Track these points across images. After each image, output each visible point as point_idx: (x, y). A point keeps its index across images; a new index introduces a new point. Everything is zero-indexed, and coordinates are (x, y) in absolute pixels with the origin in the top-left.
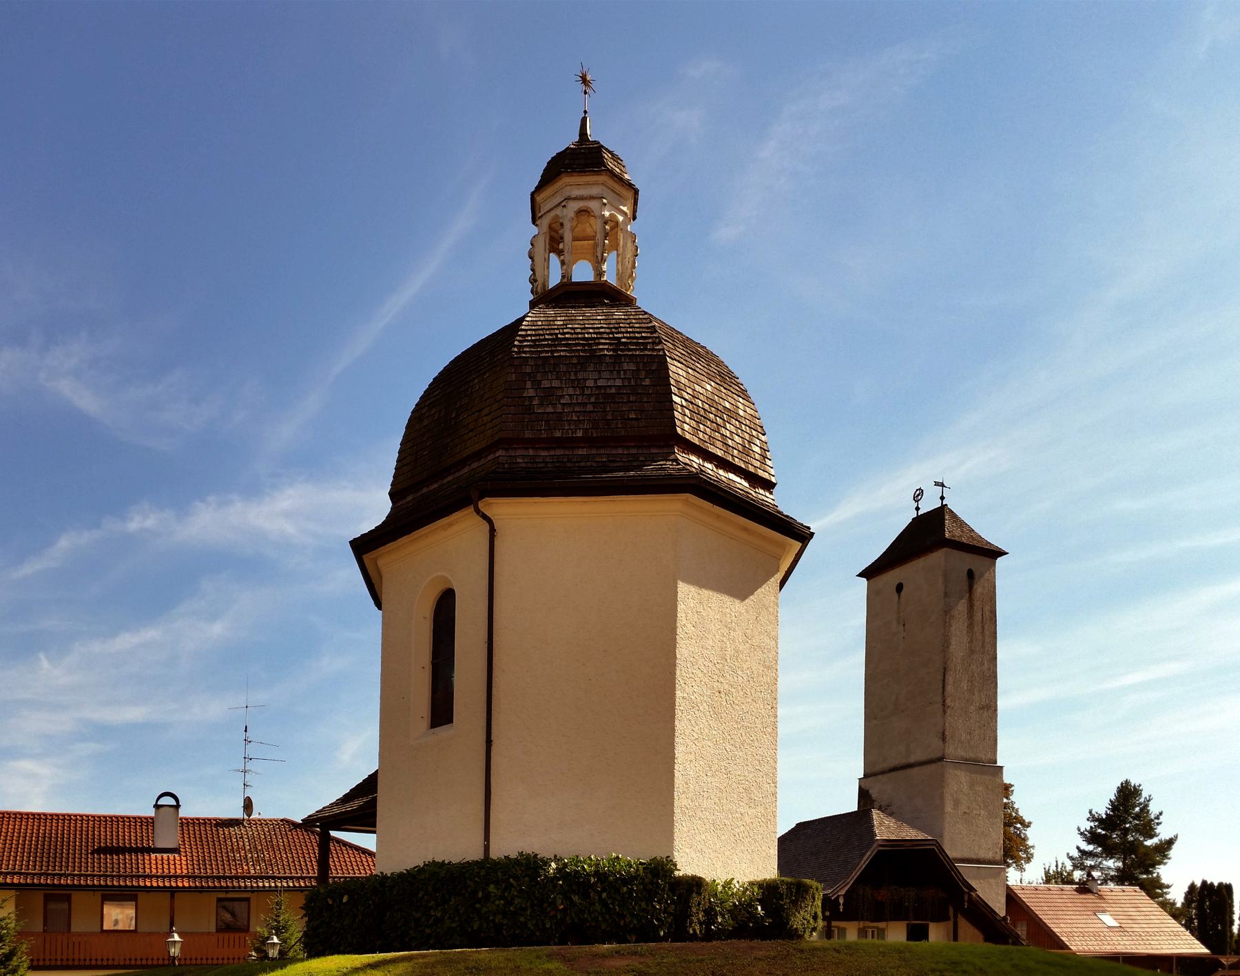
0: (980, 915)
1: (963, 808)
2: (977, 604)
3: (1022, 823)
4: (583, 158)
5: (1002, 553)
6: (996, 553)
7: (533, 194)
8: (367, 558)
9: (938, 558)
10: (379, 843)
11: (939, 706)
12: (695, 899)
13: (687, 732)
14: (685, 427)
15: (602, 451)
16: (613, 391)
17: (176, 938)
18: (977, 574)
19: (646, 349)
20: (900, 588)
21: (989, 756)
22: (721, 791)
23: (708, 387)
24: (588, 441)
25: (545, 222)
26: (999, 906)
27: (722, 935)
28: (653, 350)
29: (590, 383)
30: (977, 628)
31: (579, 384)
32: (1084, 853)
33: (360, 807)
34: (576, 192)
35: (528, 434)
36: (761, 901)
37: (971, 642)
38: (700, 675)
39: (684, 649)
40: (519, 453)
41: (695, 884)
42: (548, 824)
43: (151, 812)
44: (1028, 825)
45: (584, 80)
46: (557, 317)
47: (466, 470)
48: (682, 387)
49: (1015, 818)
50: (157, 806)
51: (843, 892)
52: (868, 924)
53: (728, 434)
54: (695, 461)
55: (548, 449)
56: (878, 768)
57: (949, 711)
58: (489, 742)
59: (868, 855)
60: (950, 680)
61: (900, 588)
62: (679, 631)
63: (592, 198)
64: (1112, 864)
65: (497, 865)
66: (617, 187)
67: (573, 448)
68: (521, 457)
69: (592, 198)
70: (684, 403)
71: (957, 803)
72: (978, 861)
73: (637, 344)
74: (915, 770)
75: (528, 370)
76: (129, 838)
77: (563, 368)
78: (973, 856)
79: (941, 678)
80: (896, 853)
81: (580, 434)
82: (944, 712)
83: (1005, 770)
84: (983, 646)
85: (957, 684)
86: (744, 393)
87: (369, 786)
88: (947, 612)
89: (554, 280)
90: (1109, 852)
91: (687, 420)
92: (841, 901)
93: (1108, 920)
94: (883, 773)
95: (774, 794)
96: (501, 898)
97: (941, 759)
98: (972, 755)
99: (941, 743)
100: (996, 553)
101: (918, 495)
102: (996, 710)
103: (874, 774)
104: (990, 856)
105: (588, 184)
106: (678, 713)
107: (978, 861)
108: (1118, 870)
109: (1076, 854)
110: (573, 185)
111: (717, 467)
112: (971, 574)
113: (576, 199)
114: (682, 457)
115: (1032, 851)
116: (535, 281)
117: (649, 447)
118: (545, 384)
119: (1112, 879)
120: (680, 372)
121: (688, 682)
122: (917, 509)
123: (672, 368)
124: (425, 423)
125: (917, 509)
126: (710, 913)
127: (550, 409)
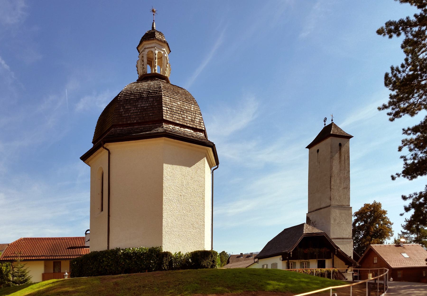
1: (337, 221)
2: (343, 154)
3: (390, 223)
4: (150, 36)
5: (351, 137)
6: (349, 137)
7: (137, 48)
9: (329, 140)
11: (329, 189)
12: (165, 259)
13: (168, 209)
14: (167, 116)
15: (142, 126)
16: (146, 107)
17: (67, 274)
18: (342, 144)
19: (157, 94)
20: (318, 151)
21: (347, 204)
22: (182, 225)
24: (138, 123)
27: (176, 268)
28: (159, 94)
29: (139, 106)
30: (343, 162)
31: (136, 106)
32: (404, 233)
34: (148, 46)
35: (120, 123)
36: (191, 258)
37: (340, 167)
38: (173, 191)
39: (166, 184)
40: (118, 128)
41: (167, 254)
42: (127, 239)
43: (84, 236)
44: (391, 224)
45: (153, 11)
46: (145, 85)
48: (167, 104)
49: (388, 222)
50: (86, 234)
51: (292, 251)
52: (303, 260)
53: (185, 117)
54: (171, 126)
55: (126, 127)
56: (312, 210)
57: (332, 190)
59: (300, 239)
60: (333, 180)
61: (318, 151)
62: (164, 178)
63: (152, 47)
64: (414, 236)
65: (112, 251)
66: (161, 43)
67: (134, 126)
68: (118, 130)
69: (152, 47)
70: (167, 109)
71: (335, 220)
72: (343, 239)
73: (154, 92)
74: (322, 210)
75: (122, 103)
76: (79, 244)
77: (132, 102)
78: (341, 237)
79: (329, 179)
80: (311, 238)
81: (135, 121)
84: (345, 168)
85: (335, 181)
86: (195, 103)
88: (332, 158)
90: (412, 232)
92: (291, 253)
93: (405, 255)
94: (313, 211)
95: (204, 225)
96: (107, 261)
97: (330, 206)
98: (341, 204)
99: (329, 201)
100: (349, 137)
101: (325, 120)
102: (349, 189)
103: (311, 212)
104: (347, 237)
105: (151, 43)
106: (164, 203)
107: (343, 239)
108: (415, 238)
109: (401, 233)
110: (147, 44)
111: (180, 127)
112: (340, 145)
113: (147, 48)
114: (165, 126)
115: (393, 232)
117: (156, 124)
118: (126, 107)
119: (414, 241)
120: (167, 100)
121: (168, 194)
122: (325, 124)
123: (163, 99)
125: (325, 124)
126: (171, 263)
127: (127, 115)
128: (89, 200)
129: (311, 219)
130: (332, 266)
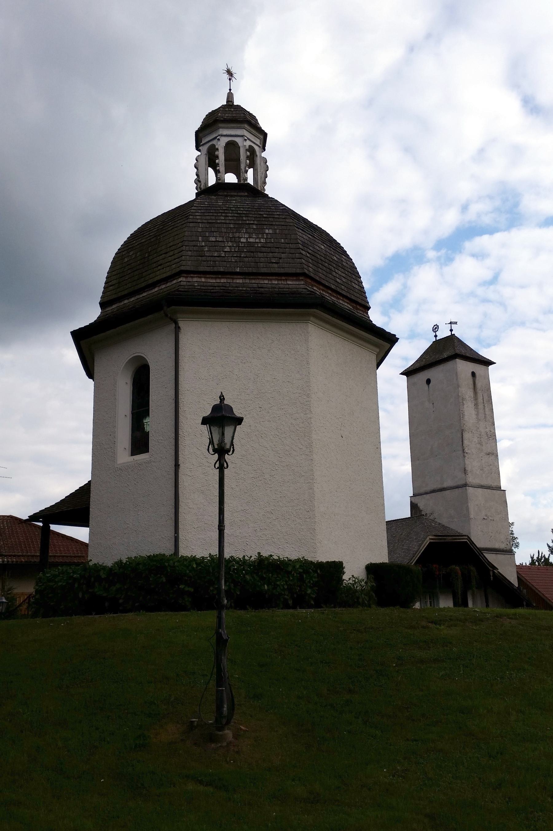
0: (500, 582)
8: (82, 343)
10: (91, 534)
11: (461, 452)
20: (428, 381)
23: (323, 247)
25: (204, 149)
26: (513, 579)
30: (481, 406)
33: (75, 508)
45: (229, 73)
47: (156, 289)
56: (422, 490)
58: (177, 466)
61: (428, 381)
67: (233, 279)
82: (464, 456)
83: (507, 493)
87: (84, 492)
89: (212, 180)
91: (311, 265)
94: (426, 493)
97: (465, 485)
101: (436, 328)
112: (473, 374)
116: (200, 181)
122: (436, 336)
124: (126, 260)
125: (436, 336)
128: (88, 458)
129: (421, 508)
130: (485, 604)
